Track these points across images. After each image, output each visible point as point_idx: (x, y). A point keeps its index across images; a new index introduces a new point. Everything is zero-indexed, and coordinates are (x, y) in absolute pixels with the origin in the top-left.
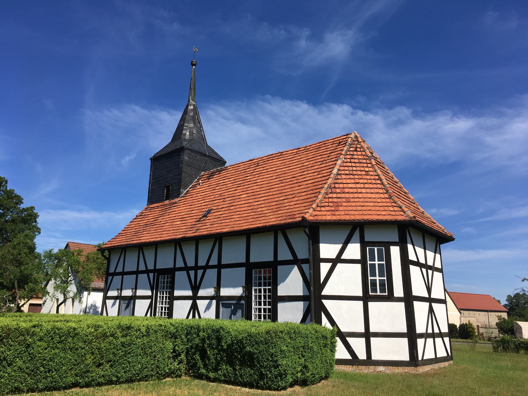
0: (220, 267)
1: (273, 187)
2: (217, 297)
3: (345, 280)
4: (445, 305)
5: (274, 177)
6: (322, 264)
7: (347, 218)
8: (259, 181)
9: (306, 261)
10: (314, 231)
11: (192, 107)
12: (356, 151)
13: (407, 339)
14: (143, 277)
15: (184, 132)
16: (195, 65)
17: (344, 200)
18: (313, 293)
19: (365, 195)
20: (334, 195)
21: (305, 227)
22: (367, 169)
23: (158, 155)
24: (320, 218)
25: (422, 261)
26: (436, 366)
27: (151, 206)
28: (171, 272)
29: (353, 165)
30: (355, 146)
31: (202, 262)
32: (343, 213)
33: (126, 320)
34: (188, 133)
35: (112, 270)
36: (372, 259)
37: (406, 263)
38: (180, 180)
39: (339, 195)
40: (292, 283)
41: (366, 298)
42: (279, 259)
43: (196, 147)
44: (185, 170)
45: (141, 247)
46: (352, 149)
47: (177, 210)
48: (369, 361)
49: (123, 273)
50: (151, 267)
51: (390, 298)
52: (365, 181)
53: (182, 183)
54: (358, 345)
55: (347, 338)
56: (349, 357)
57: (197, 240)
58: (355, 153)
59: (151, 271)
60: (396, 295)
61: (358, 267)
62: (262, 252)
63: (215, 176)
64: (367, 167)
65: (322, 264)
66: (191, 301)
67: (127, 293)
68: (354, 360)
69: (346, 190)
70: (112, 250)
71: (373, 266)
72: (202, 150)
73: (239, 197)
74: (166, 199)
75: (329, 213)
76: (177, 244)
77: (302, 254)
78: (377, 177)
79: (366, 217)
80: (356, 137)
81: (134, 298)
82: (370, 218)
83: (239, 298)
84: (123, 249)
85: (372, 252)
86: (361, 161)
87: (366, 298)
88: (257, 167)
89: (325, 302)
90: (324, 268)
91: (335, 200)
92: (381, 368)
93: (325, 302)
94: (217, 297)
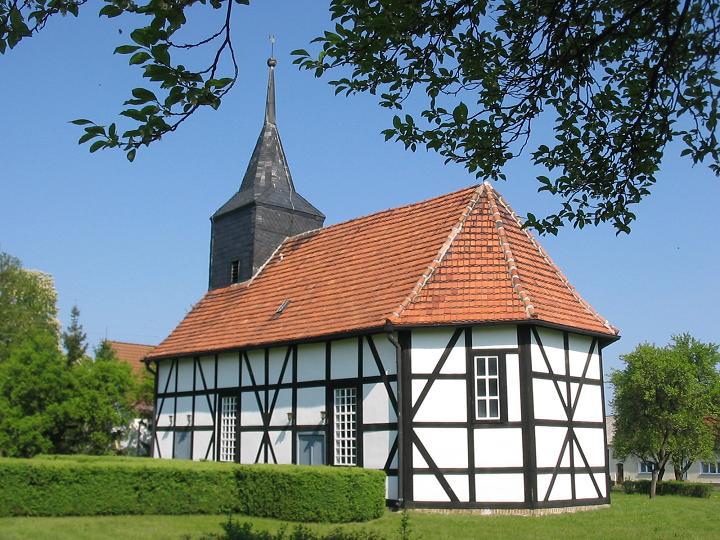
0: (295, 385)
1: (370, 268)
2: (294, 428)
3: (445, 401)
4: (602, 430)
5: (374, 253)
6: (414, 382)
7: (447, 318)
8: (354, 258)
9: (393, 378)
10: (404, 336)
11: (270, 134)
12: (481, 214)
13: (414, 466)
14: (201, 400)
15: (258, 175)
16: (274, 65)
17: (449, 292)
18: (401, 419)
19: (479, 284)
20: (437, 286)
21: (390, 332)
22: (490, 243)
23: (221, 213)
24: (409, 320)
25: (559, 370)
26: (572, 510)
27: (215, 292)
28: (235, 393)
29: (473, 236)
30: (481, 206)
31: (273, 380)
32: (442, 312)
33: (182, 465)
34: (263, 177)
35: (161, 390)
36: (482, 371)
37: (527, 375)
38: (252, 252)
39: (443, 286)
40: (377, 404)
41: (471, 424)
42: (291, 390)
43: (274, 199)
44: (258, 236)
45: (197, 358)
46: (476, 212)
47: (246, 300)
48: (473, 504)
49: (176, 395)
50: (211, 386)
51: (504, 422)
52: (485, 262)
53: (255, 258)
54: (460, 485)
55: (445, 476)
56: (448, 499)
57: (267, 349)
58: (479, 218)
59: (211, 391)
60: (510, 419)
61: (463, 383)
62: (345, 365)
63: (302, 246)
64: (492, 239)
65: (414, 382)
66: (262, 433)
67: (182, 420)
68: (454, 503)
69: (455, 277)
70: (159, 361)
71: (482, 383)
72: (285, 203)
73: (326, 283)
74: (235, 282)
75: (425, 312)
76: (243, 353)
77: (390, 369)
78: (502, 256)
79: (471, 317)
80: (485, 191)
81: (191, 429)
82: (477, 317)
83: (318, 428)
84: (175, 360)
85: (481, 363)
86: (485, 230)
87: (471, 424)
88: (358, 234)
89: (416, 430)
90: (417, 386)
91: (437, 293)
92: (487, 512)
93: (416, 430)
94: (294, 428)
